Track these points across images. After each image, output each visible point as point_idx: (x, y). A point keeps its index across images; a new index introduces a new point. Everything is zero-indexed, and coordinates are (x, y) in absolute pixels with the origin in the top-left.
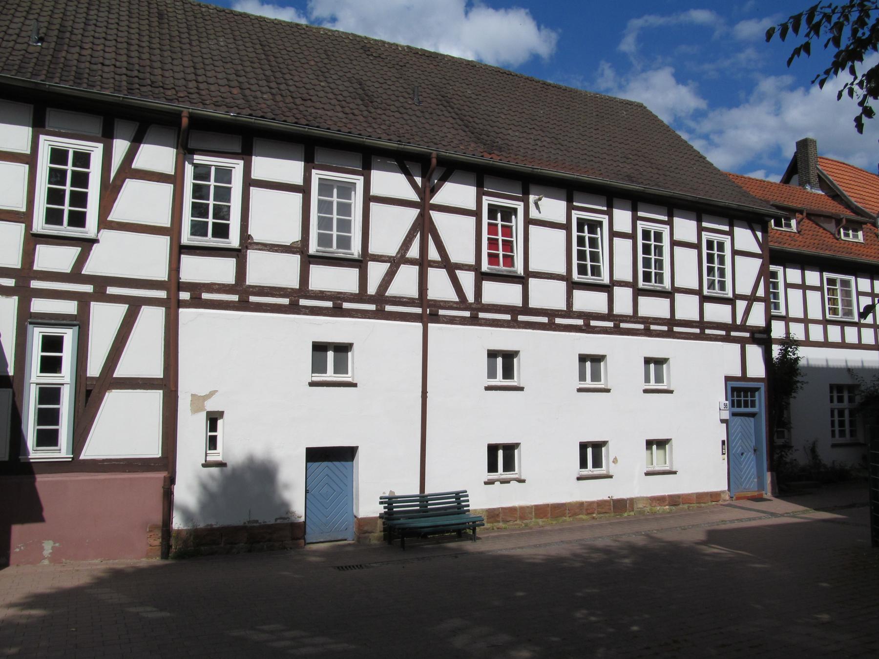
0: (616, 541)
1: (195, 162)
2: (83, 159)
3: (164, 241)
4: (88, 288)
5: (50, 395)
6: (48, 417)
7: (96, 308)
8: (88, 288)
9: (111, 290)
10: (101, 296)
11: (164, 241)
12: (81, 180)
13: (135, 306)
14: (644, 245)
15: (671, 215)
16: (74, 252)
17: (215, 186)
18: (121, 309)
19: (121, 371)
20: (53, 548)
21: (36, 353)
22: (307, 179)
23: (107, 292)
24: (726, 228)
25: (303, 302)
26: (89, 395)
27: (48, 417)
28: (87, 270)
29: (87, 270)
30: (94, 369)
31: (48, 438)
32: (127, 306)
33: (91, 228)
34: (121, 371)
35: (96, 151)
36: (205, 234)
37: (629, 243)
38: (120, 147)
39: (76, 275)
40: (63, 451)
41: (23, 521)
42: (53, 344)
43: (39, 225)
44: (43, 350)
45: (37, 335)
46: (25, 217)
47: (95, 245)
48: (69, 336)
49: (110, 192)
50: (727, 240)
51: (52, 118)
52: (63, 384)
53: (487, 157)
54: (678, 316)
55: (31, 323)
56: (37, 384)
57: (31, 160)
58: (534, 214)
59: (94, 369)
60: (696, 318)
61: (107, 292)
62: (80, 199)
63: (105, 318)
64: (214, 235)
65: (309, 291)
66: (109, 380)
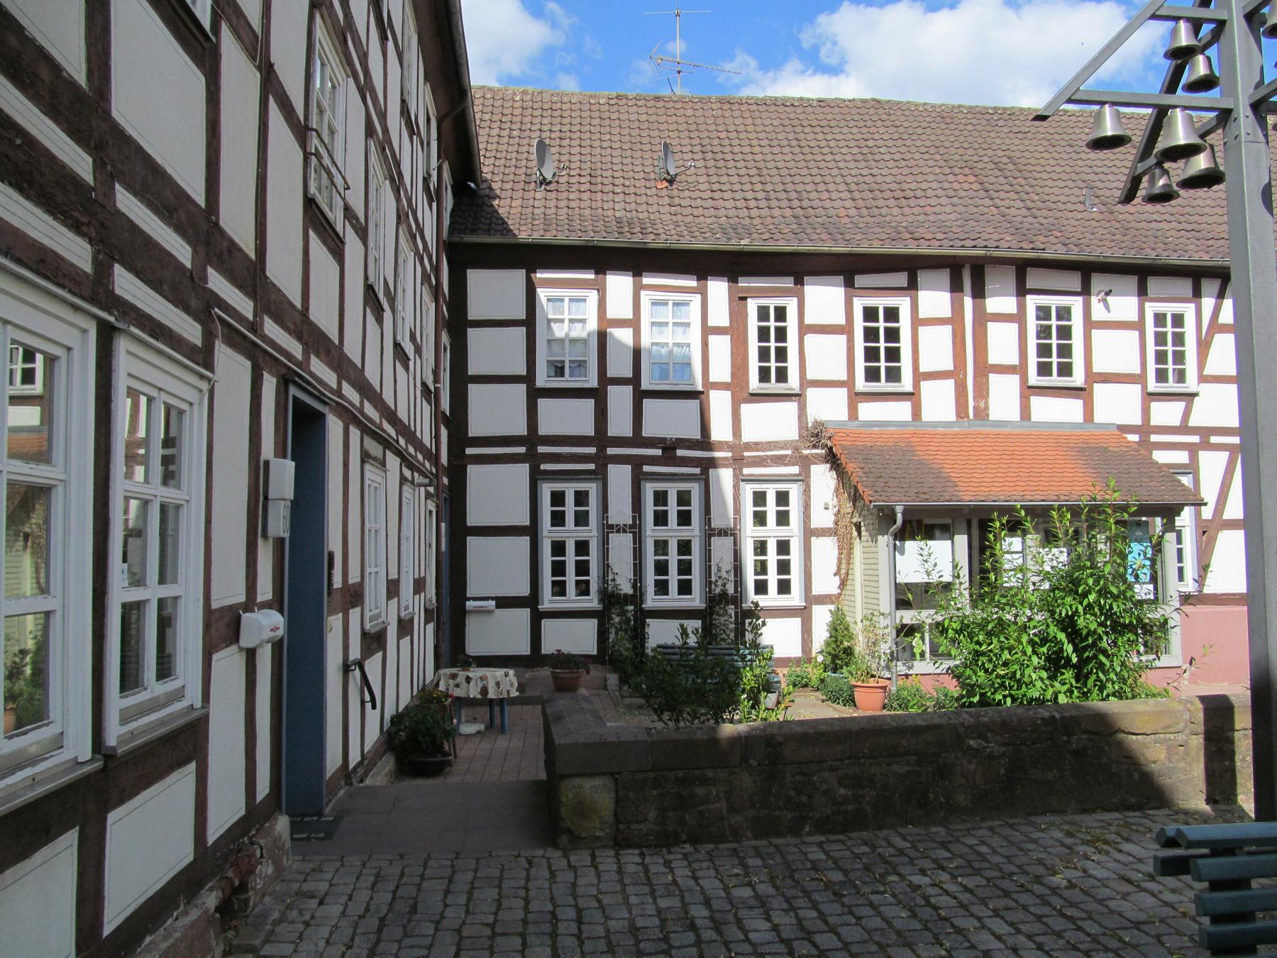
2: (1178, 320)
3: (522, 388)
4: (1195, 439)
7: (1203, 455)
8: (1195, 439)
9: (1214, 439)
11: (522, 388)
12: (1179, 339)
14: (1157, 334)
15: (799, 282)
16: (1179, 406)
17: (877, 321)
22: (1022, 307)
24: (694, 283)
29: (1193, 422)
33: (1191, 383)
35: (1188, 310)
36: (1050, 374)
37: (1013, 328)
39: (1184, 429)
43: (861, 384)
44: (553, 575)
46: (1140, 379)
47: (1196, 399)
50: (791, 305)
53: (865, 244)
54: (543, 430)
57: (1139, 326)
58: (1098, 312)
60: (522, 430)
62: (1179, 357)
64: (1059, 375)
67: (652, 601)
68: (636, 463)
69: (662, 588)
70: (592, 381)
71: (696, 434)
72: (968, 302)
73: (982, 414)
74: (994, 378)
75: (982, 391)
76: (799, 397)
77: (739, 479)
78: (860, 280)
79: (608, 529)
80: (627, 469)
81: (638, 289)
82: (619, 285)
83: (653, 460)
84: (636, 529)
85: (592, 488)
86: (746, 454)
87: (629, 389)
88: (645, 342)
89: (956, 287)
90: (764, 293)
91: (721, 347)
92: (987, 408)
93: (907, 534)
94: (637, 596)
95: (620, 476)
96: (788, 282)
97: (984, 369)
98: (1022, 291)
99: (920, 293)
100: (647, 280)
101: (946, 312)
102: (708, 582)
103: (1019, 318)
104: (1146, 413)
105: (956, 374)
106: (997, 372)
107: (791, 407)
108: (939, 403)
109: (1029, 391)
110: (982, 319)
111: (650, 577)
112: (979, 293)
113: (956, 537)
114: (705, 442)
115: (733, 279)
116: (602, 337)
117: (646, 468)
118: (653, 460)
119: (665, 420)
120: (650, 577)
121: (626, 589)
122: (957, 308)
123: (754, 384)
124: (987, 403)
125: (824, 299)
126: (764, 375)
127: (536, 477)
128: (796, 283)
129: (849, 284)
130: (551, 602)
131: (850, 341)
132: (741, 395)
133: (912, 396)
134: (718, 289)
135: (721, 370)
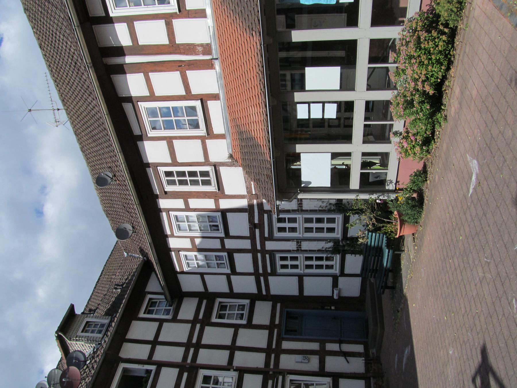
15: (148, 165)
50: (162, 170)
67: (338, 235)
68: (263, 240)
69: (331, 230)
70: (225, 254)
71: (246, 215)
72: (129, 59)
73: (207, 49)
74: (180, 40)
75: (189, 49)
76: (216, 166)
77: (271, 238)
78: (137, 131)
79: (299, 250)
80: (267, 243)
81: (173, 236)
82: (173, 243)
83: (262, 233)
84: (299, 241)
85: (278, 256)
86: (254, 193)
87: (177, 23)
88: (198, 234)
89: (121, 70)
90: (159, 182)
91: (194, 203)
92: (202, 45)
93: (297, 87)
94: (336, 241)
95: (270, 245)
96: (150, 171)
97: (173, 47)
98: (108, 20)
99: (133, 95)
100: (168, 232)
101: (140, 76)
102: (330, 211)
103: (130, 20)
104: (222, 137)
105: (182, 67)
106: (174, 38)
107: (223, 170)
108: (205, 81)
109: (250, 325)
110: (138, 49)
111: (325, 235)
112: (120, 51)
113: (297, 151)
114: (249, 209)
115: (157, 197)
116: (200, 250)
117: (266, 235)
118: (262, 233)
119: (239, 225)
120: (325, 235)
121: (331, 244)
122: (137, 68)
123: (212, 188)
124: (198, 45)
125: (154, 152)
126: (207, 183)
127: (274, 273)
128: (149, 167)
129: (141, 138)
130: (336, 270)
131: (176, 138)
132: (220, 193)
133: (203, 99)
134: (163, 203)
135: (210, 204)
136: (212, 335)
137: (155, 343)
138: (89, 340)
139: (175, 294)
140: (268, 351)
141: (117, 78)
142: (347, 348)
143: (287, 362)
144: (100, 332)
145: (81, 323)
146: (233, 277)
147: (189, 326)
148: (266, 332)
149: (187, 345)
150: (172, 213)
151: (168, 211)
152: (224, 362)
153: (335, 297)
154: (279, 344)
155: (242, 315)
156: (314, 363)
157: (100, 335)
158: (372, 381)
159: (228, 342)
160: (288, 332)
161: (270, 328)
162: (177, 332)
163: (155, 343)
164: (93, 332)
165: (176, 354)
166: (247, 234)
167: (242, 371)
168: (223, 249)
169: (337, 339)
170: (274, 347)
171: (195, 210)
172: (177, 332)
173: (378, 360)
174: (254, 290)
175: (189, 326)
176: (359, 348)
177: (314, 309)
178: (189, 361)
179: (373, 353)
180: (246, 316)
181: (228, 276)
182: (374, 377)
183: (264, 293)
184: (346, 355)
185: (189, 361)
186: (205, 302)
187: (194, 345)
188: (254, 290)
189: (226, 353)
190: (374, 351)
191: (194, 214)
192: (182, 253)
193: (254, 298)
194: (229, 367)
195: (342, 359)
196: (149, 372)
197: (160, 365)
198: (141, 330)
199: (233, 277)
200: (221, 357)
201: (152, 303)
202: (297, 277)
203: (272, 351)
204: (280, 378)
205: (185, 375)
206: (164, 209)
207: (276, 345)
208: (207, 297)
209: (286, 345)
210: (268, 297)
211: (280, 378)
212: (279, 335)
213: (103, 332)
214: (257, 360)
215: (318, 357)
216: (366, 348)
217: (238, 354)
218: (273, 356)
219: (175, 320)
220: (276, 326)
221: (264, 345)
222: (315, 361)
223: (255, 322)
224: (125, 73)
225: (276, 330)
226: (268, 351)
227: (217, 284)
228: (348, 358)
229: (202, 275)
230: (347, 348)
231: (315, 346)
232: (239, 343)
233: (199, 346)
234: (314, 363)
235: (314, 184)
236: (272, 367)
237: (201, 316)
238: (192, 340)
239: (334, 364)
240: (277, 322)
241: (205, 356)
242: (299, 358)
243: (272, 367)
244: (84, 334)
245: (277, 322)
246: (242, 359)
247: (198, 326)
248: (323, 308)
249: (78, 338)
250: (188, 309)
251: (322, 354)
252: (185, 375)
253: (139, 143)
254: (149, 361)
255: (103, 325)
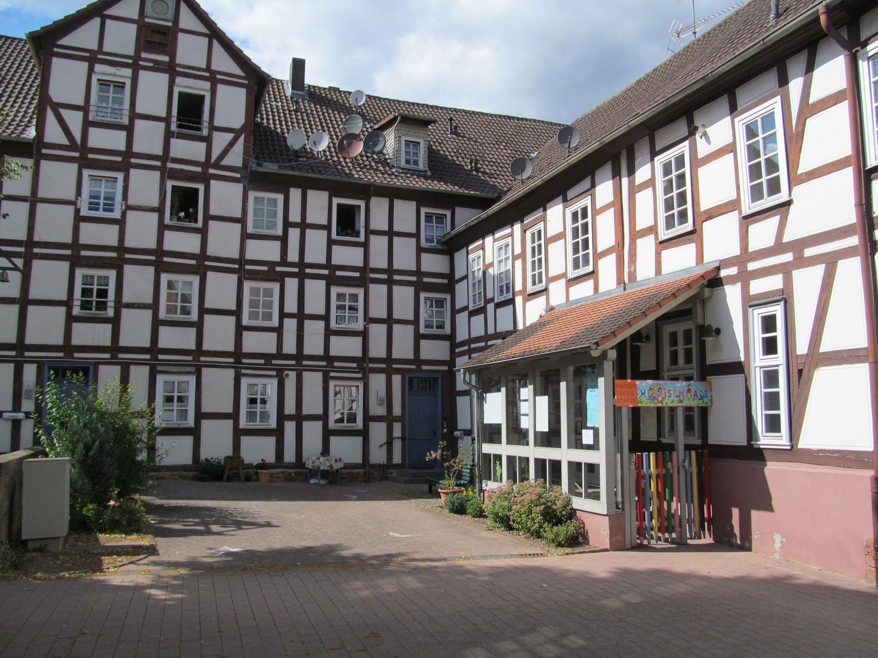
0: (210, 549)
1: (870, 54)
2: (354, 297)
5: (771, 377)
6: (772, 401)
7: (798, 275)
10: (801, 262)
13: (831, 261)
15: (545, 210)
18: (819, 270)
19: (826, 346)
20: (782, 542)
21: (758, 336)
23: (749, 269)
25: (752, 266)
26: (800, 375)
27: (772, 401)
28: (786, 239)
30: (802, 347)
31: (773, 424)
32: (823, 266)
34: (826, 346)
38: (795, 86)
40: (781, 440)
41: (759, 508)
42: (769, 323)
45: (757, 315)
47: (792, 207)
48: (778, 310)
49: (794, 140)
51: (743, 96)
52: (778, 366)
55: (750, 306)
56: (761, 367)
59: (802, 347)
61: (749, 269)
63: (807, 283)
65: (741, 254)
66: (819, 357)
78: (571, 194)
81: (495, 241)
89: (616, 174)
91: (518, 263)
96: (539, 213)
100: (497, 235)
109: (418, 337)
112: (631, 172)
116: (484, 273)
136: (404, 296)
137: (391, 234)
138: (397, 151)
139: (454, 245)
140: (389, 359)
141: (607, 169)
142: (397, 446)
143: (378, 381)
144: (408, 162)
145: (416, 137)
146: (563, 281)
147: (414, 268)
148: (411, 356)
149: (390, 270)
150: (509, 240)
151: (511, 235)
152: (372, 314)
153: (456, 433)
154: (398, 371)
155: (432, 327)
156: (378, 410)
157: (403, 164)
158: (361, 471)
159: (396, 315)
160: (411, 381)
161: (417, 360)
162: (405, 255)
163: (391, 234)
164: (407, 153)
165: (379, 260)
166: (124, 311)
167: (364, 334)
168: (487, 301)
169: (407, 435)
170: (394, 366)
171: (513, 266)
172: (405, 255)
173: (385, 478)
174: (459, 339)
175: (414, 268)
176: (397, 459)
177: (443, 410)
178: (372, 275)
179: (391, 473)
180: (429, 331)
181: (564, 275)
182: (365, 473)
183: (457, 350)
184: (389, 443)
185: (372, 275)
186: (445, 281)
187: (391, 277)
188: (459, 339)
189: (384, 315)
190: (394, 475)
191: (510, 266)
192: (481, 252)
193: (451, 338)
194: (369, 320)
195: (384, 439)
196: (358, 234)
197: (365, 245)
198: (406, 214)
199: (563, 281)
200: (379, 310)
201: (441, 219)
202: (655, 368)
203: (389, 365)
204: (360, 376)
205: (357, 274)
206: (546, 214)
207: (397, 369)
208: (449, 283)
209: (397, 379)
210: (453, 355)
211: (360, 376)
212: (409, 371)
213: (408, 166)
214: (378, 349)
215: (385, 414)
216: (396, 466)
217: (383, 328)
218: (384, 366)
219: (420, 250)
220: (419, 366)
221: (395, 355)
222: (381, 411)
223: (423, 342)
224: (613, 178)
225: (414, 367)
226: (389, 359)
227: (463, 295)
228: (385, 447)
229: (466, 277)
230: (397, 446)
231: (397, 411)
232: (396, 327)
233: (390, 283)
234: (378, 410)
235: (486, 406)
236: (371, 365)
237: (426, 280)
238: (397, 274)
239: (378, 431)
240: (424, 367)
241: (378, 292)
242: (383, 393)
243: (371, 365)
244: (403, 143)
245: (424, 367)
246: (378, 332)
247: (414, 279)
248: (444, 419)
249: (398, 138)
250: (433, 263)
251: (389, 419)
252: (357, 274)
253: (561, 198)
254: (369, 232)
255: (416, 163)
